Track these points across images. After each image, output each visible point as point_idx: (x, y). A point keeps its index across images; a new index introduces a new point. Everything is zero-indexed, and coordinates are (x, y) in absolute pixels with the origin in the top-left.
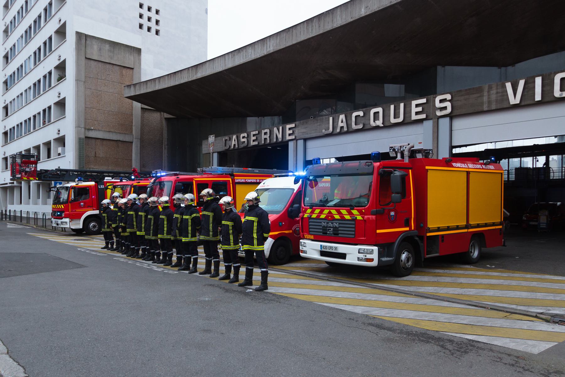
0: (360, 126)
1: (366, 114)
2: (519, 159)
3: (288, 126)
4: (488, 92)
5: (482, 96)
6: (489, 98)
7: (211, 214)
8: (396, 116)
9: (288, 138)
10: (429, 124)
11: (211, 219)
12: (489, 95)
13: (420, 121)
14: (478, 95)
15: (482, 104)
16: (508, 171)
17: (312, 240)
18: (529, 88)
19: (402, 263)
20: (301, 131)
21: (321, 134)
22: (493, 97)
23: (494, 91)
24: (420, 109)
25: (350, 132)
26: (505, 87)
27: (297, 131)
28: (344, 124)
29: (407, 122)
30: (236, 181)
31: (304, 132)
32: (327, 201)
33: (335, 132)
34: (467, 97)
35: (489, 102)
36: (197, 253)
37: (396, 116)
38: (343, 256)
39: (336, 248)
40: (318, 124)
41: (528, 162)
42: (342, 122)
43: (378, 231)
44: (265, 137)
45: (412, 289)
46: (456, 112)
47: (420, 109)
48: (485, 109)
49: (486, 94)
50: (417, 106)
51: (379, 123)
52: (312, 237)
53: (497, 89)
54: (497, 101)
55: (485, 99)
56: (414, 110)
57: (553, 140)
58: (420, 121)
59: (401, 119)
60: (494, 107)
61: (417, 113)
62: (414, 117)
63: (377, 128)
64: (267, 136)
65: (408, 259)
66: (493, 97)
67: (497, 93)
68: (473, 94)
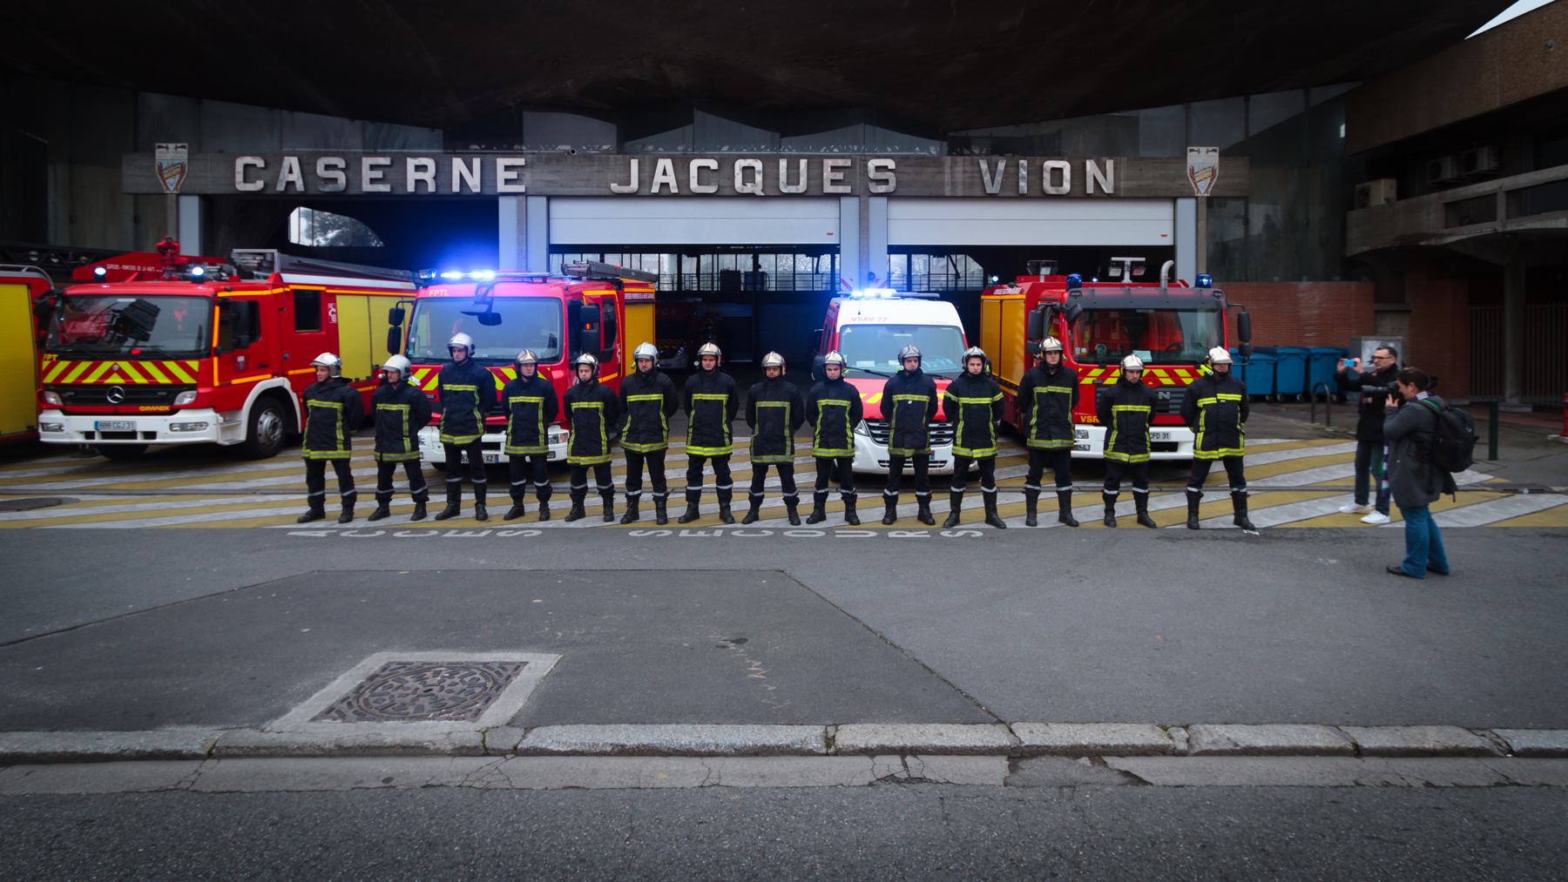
0: (712, 189)
1: (726, 163)
3: (502, 162)
7: (787, 404)
8: (793, 178)
10: (850, 205)
11: (405, 417)
13: (837, 197)
15: (942, 184)
17: (1095, 424)
18: (1012, 175)
19: (261, 439)
20: (543, 177)
22: (959, 177)
23: (959, 169)
25: (685, 195)
27: (527, 175)
28: (671, 179)
29: (814, 194)
30: (627, 296)
33: (644, 191)
35: (953, 184)
37: (793, 178)
38: (1173, 447)
39: (1166, 435)
41: (727, 261)
42: (665, 173)
43: (235, 382)
44: (420, 176)
45: (252, 484)
46: (902, 192)
47: (379, 174)
49: (947, 170)
50: (507, 168)
51: (757, 187)
52: (1095, 419)
54: (964, 183)
55: (947, 178)
56: (502, 175)
58: (837, 197)
59: (802, 187)
60: (960, 193)
61: (507, 181)
62: (828, 189)
64: (428, 176)
65: (274, 426)
66: (959, 177)
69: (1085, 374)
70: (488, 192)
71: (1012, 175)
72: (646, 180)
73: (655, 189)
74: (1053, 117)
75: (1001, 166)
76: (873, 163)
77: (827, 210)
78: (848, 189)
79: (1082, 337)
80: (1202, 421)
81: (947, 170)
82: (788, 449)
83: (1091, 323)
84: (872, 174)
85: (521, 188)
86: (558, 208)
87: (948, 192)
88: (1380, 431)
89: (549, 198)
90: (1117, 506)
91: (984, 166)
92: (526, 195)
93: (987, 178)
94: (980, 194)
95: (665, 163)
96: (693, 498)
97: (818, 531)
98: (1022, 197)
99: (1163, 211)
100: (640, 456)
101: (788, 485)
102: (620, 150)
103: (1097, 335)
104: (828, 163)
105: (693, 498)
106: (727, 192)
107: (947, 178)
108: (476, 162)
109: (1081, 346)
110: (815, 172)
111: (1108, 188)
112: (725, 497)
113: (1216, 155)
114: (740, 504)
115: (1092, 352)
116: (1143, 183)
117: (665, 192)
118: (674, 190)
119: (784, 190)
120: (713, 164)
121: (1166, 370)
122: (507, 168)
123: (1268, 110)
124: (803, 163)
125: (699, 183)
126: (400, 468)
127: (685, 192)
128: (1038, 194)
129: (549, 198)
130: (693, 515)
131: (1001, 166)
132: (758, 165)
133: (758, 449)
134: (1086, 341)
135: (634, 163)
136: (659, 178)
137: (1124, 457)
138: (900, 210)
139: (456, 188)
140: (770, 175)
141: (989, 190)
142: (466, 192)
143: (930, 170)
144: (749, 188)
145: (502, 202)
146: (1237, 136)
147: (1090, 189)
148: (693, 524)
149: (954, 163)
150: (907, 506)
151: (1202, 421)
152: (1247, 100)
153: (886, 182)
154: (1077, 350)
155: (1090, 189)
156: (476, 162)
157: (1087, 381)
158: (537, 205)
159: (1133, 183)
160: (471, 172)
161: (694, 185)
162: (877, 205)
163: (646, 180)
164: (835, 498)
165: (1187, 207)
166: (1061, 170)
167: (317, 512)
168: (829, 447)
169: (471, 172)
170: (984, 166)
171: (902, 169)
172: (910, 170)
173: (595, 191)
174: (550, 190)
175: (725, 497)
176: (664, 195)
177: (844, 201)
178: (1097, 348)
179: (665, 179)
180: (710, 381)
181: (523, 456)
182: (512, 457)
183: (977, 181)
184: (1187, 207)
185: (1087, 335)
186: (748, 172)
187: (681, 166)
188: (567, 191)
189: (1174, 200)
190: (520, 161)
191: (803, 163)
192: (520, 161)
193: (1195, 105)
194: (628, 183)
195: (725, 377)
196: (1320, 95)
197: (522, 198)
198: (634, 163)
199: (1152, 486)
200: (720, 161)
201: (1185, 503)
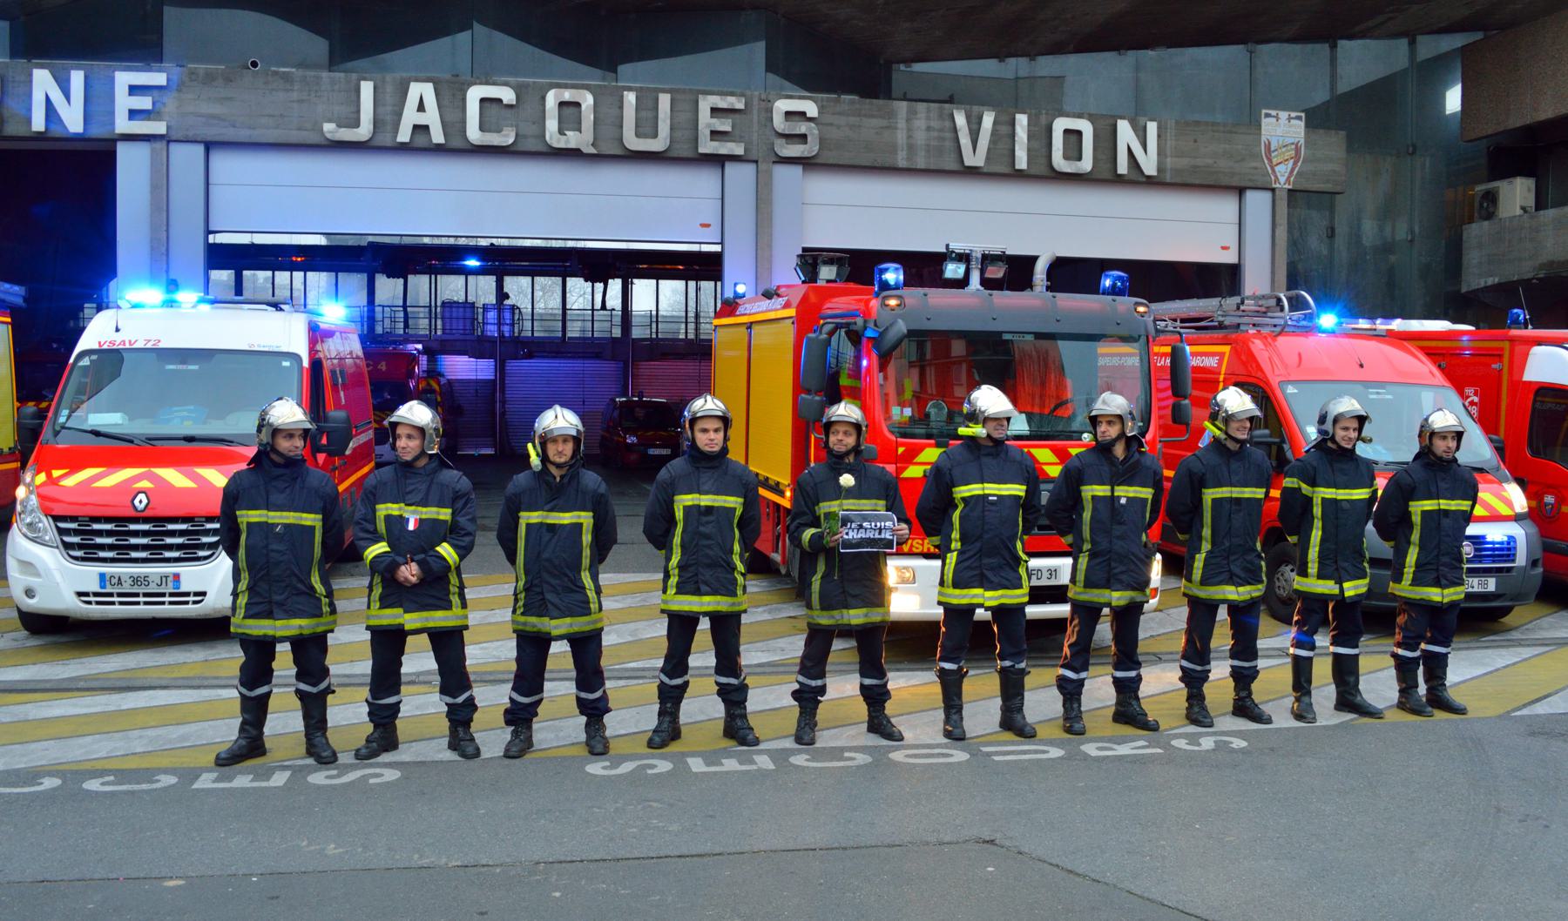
0: (507, 138)
1: (530, 97)
2: (269, 273)
3: (124, 78)
4: (908, 120)
5: (892, 128)
6: (909, 137)
8: (646, 127)
9: (123, 125)
10: (742, 176)
12: (909, 130)
14: (884, 123)
15: (894, 149)
16: (405, 306)
20: (206, 109)
21: (313, 138)
22: (921, 137)
23: (920, 123)
24: (144, 103)
26: (1013, 123)
28: (432, 118)
29: (683, 156)
31: (213, 117)
32: (835, 377)
34: (852, 120)
35: (911, 148)
36: (1142, 584)
37: (646, 127)
40: (295, 96)
47: (144, 103)
48: (902, 163)
49: (902, 124)
50: (134, 90)
53: (928, 118)
54: (928, 148)
56: (124, 102)
57: (320, 241)
58: (719, 161)
60: (921, 164)
61: (133, 114)
62: (707, 146)
63: (573, 154)
66: (921, 137)
67: (929, 129)
68: (872, 116)
69: (910, 457)
70: (97, 132)
71: (1004, 136)
72: (388, 117)
73: (404, 136)
74: (1057, 49)
75: (988, 120)
76: (783, 105)
77: (703, 182)
78: (739, 150)
79: (900, 391)
80: (677, 540)
81: (902, 124)
82: (455, 600)
83: (921, 365)
84: (779, 123)
85: (159, 128)
86: (227, 165)
87: (902, 162)
88: (433, 548)
89: (209, 146)
90: (686, 706)
91: (960, 120)
92: (165, 139)
93: (965, 141)
94: (954, 166)
95: (421, 90)
96: (671, 698)
97: (384, 772)
98: (1019, 176)
99: (1225, 207)
100: (1211, 607)
101: (454, 677)
102: (336, 59)
103: (931, 386)
104: (706, 104)
105: (671, 698)
106: (531, 145)
107: (901, 137)
108: (77, 78)
109: (902, 405)
110: (684, 117)
111: (1149, 166)
112: (314, 710)
113: (1302, 124)
114: (349, 714)
115: (922, 418)
116: (1199, 162)
117: (421, 141)
118: (438, 137)
119: (474, 134)
120: (507, 95)
121: (1055, 450)
122: (134, 90)
123: (1363, 61)
124: (665, 100)
125: (483, 127)
126: (559, 649)
127: (457, 143)
128: (1043, 170)
129: (209, 146)
130: (668, 732)
131: (988, 120)
132: (587, 100)
133: (534, 599)
134: (908, 395)
135: (367, 89)
136: (410, 117)
137: (1434, 594)
138: (827, 189)
139: (38, 124)
140: (609, 119)
141: (970, 160)
142: (56, 131)
143: (875, 122)
144: (572, 140)
145: (124, 152)
146: (1321, 96)
147: (1123, 167)
148: (674, 748)
149: (912, 114)
150: (982, 691)
151: (677, 540)
152: (1334, 47)
153: (803, 138)
154: (896, 411)
155: (1123, 167)
156: (77, 78)
157: (914, 472)
158: (187, 158)
159: (1184, 162)
160: (67, 95)
161: (474, 134)
162: (786, 176)
163: (388, 117)
164: (843, 687)
165: (1258, 202)
166: (1079, 133)
167: (251, 746)
168: (697, 592)
169: (67, 95)
170: (960, 120)
171: (828, 118)
172: (842, 120)
173: (295, 136)
174: (213, 133)
175: (314, 710)
176: (420, 146)
177: (730, 168)
178: (930, 408)
179: (421, 119)
180: (407, 479)
181: (971, 609)
182: (950, 610)
183: (949, 144)
184: (1258, 202)
185: (910, 385)
186: (569, 109)
187: (451, 97)
188: (243, 135)
189: (1241, 191)
190: (159, 79)
191: (665, 100)
192: (159, 79)
193: (1265, 49)
194: (356, 123)
195: (591, 479)
196: (1430, 46)
197: (160, 145)
198: (367, 89)
199: (1457, 642)
200: (520, 91)
201: (938, 689)
